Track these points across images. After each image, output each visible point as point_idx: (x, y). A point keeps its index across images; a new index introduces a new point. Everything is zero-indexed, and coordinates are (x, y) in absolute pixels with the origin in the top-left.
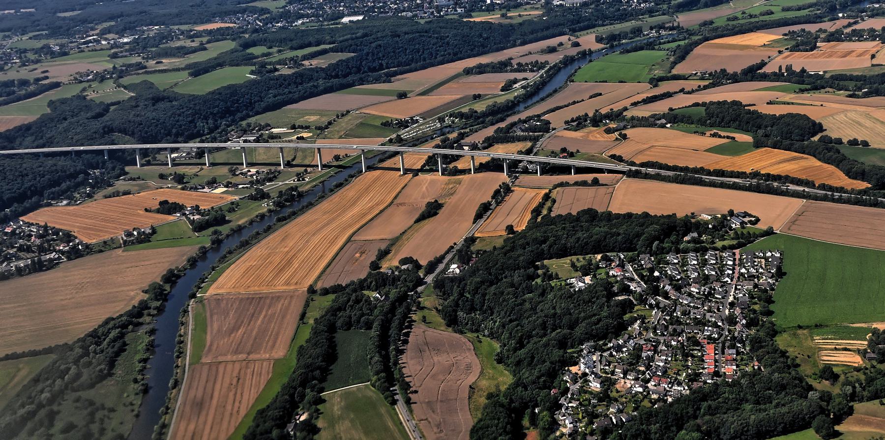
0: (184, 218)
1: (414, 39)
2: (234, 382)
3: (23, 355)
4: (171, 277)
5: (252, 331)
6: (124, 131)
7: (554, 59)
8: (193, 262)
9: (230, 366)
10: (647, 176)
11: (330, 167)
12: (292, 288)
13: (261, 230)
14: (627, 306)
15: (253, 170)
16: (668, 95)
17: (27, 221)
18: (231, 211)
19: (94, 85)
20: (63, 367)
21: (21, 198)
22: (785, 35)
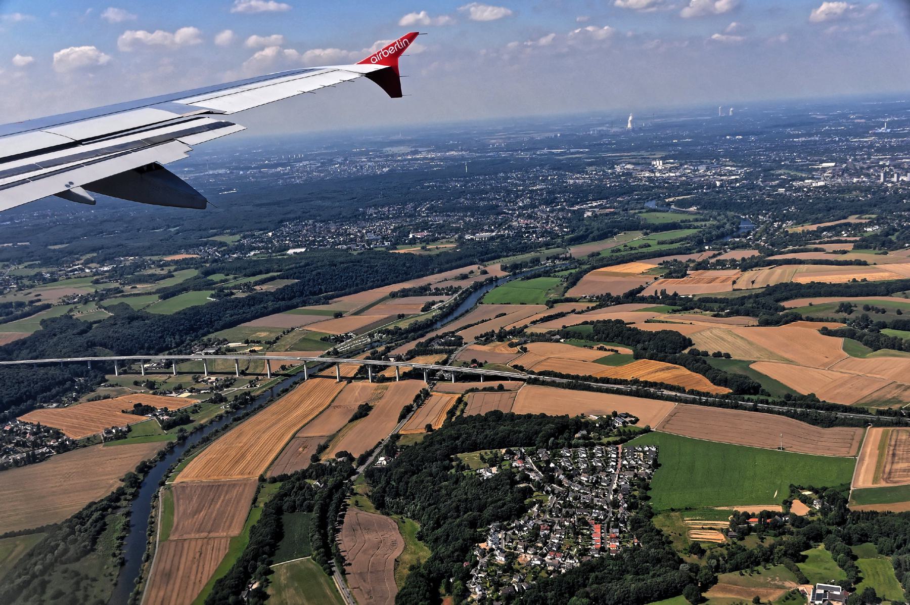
0: (155, 418)
1: (348, 267)
2: (198, 554)
3: (20, 533)
4: (144, 468)
5: (212, 513)
6: (104, 345)
7: (466, 284)
8: (162, 455)
9: (193, 543)
10: (544, 383)
14: (528, 492)
15: (213, 378)
16: (561, 315)
18: (195, 412)
19: (80, 306)
20: (53, 544)
21: (18, 401)
22: (660, 264)
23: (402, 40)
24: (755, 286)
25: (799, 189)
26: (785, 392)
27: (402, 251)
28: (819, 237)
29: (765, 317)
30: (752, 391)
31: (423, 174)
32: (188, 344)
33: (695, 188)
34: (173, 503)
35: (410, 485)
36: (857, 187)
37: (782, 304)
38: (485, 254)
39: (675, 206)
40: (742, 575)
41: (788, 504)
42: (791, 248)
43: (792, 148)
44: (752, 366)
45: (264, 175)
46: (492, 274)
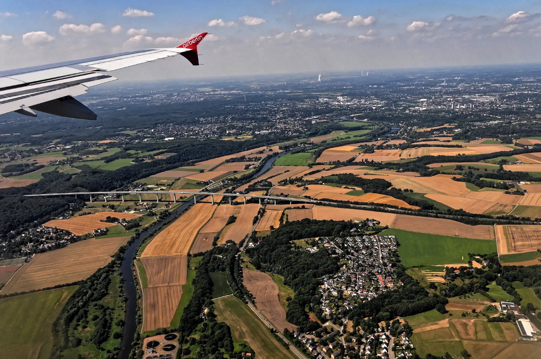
0: (120, 224)
1: (201, 147)
2: (166, 295)
3: (63, 286)
4: (122, 250)
5: (167, 273)
6: (82, 186)
7: (264, 156)
8: (130, 243)
9: (162, 289)
10: (325, 205)
11: (179, 202)
12: (179, 254)
13: (157, 229)
14: (337, 259)
15: (145, 203)
16: (318, 171)
17: (46, 226)
19: (60, 166)
20: (85, 291)
21: (41, 216)
23: (199, 36)
24: (411, 157)
25: (415, 111)
26: (447, 209)
27: (226, 139)
28: (433, 134)
29: (424, 172)
30: (430, 208)
31: (222, 102)
32: (126, 186)
33: (363, 110)
34: (143, 268)
35: (272, 256)
36: (441, 111)
37: (428, 166)
38: (268, 141)
39: (356, 118)
40: (460, 298)
41: (470, 263)
42: (421, 139)
43: (403, 91)
44: (425, 196)
45: (138, 101)
46: (274, 151)
